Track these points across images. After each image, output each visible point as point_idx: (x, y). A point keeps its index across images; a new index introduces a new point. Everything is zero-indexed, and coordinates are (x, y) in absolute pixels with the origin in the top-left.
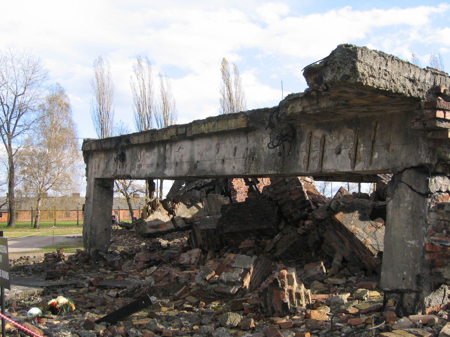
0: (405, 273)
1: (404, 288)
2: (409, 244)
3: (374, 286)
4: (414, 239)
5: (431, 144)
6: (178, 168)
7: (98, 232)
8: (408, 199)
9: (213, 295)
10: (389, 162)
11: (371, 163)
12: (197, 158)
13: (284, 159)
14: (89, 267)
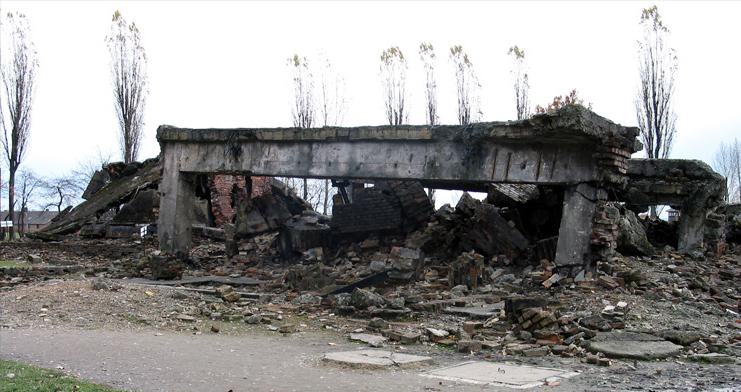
3: (363, 132)
7: (181, 232)
12: (359, 160)
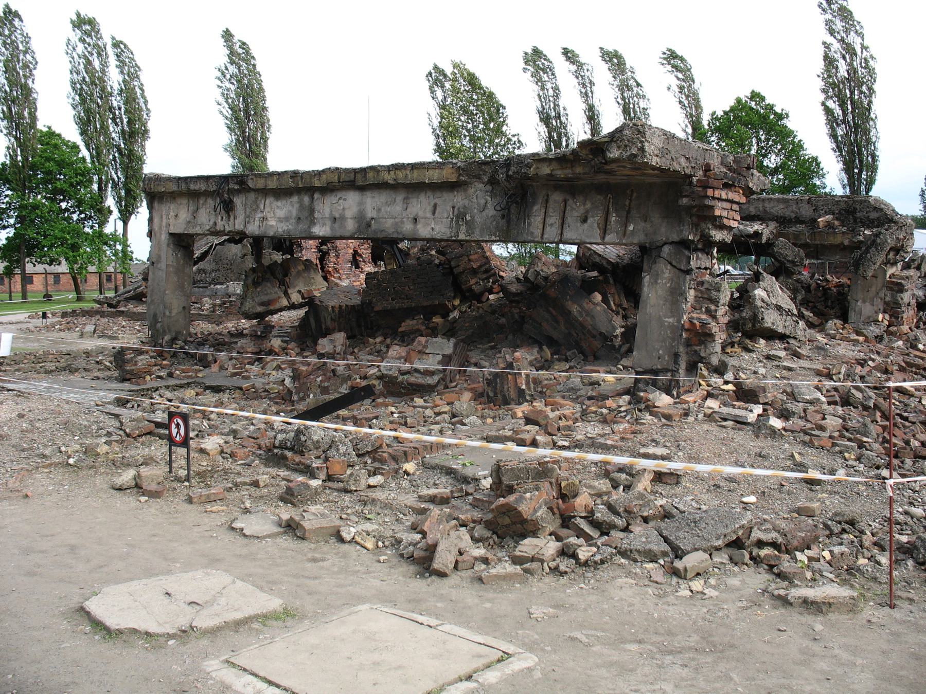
0: (661, 352)
6: (336, 225)
7: (174, 312)
8: (667, 275)
9: (404, 388)
10: (646, 235)
11: (624, 235)
12: (370, 213)
13: (509, 222)
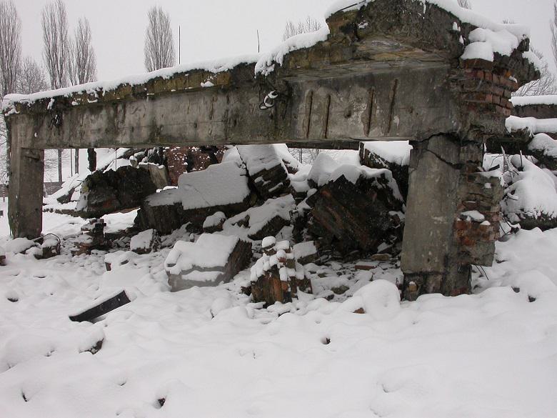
0: (430, 253)
1: (429, 270)
2: (436, 220)
4: (443, 215)
5: (464, 108)
6: (134, 134)
12: (160, 122)
14: (462, 213)
